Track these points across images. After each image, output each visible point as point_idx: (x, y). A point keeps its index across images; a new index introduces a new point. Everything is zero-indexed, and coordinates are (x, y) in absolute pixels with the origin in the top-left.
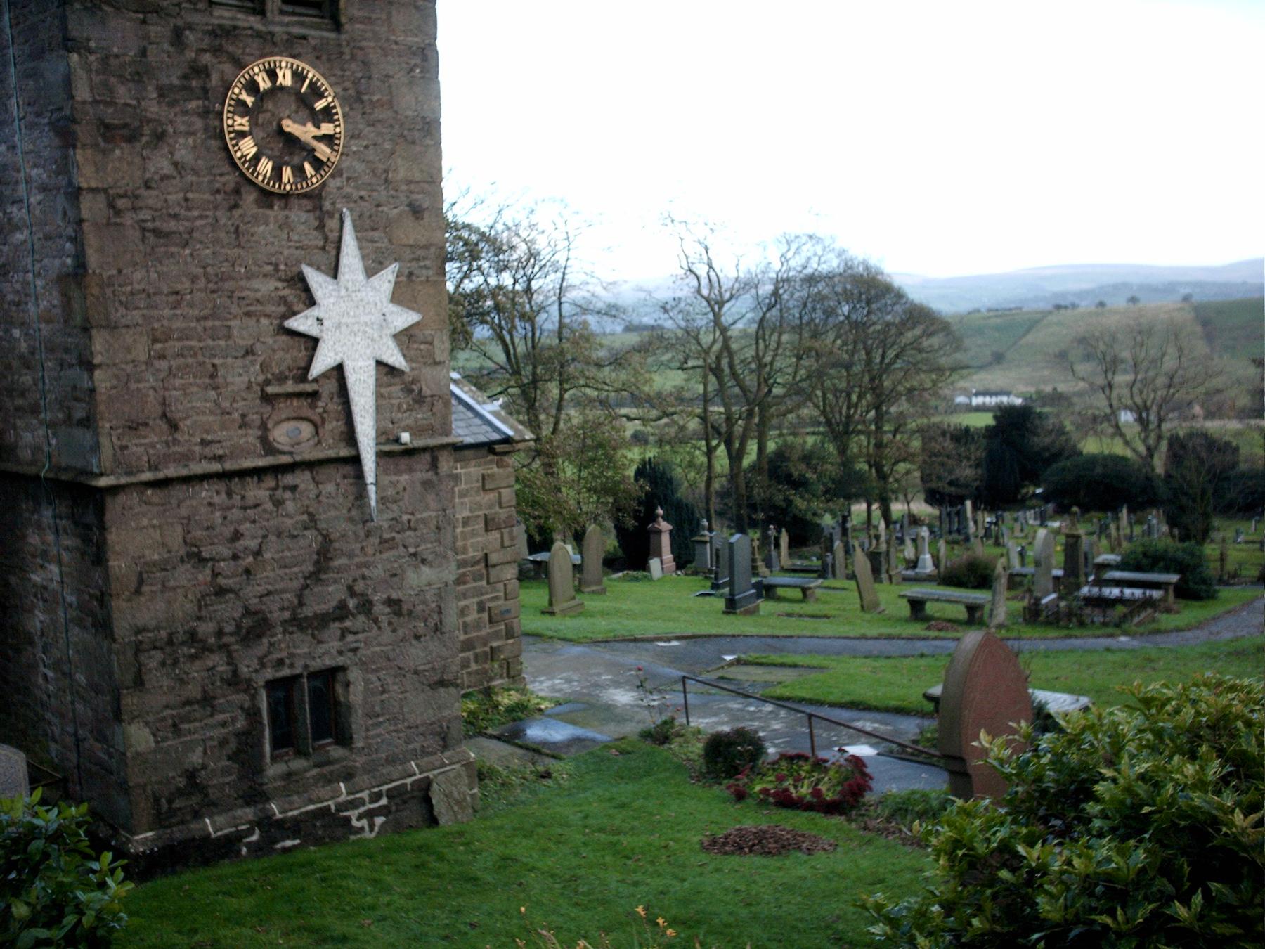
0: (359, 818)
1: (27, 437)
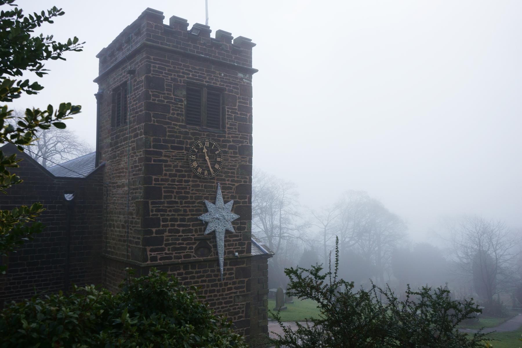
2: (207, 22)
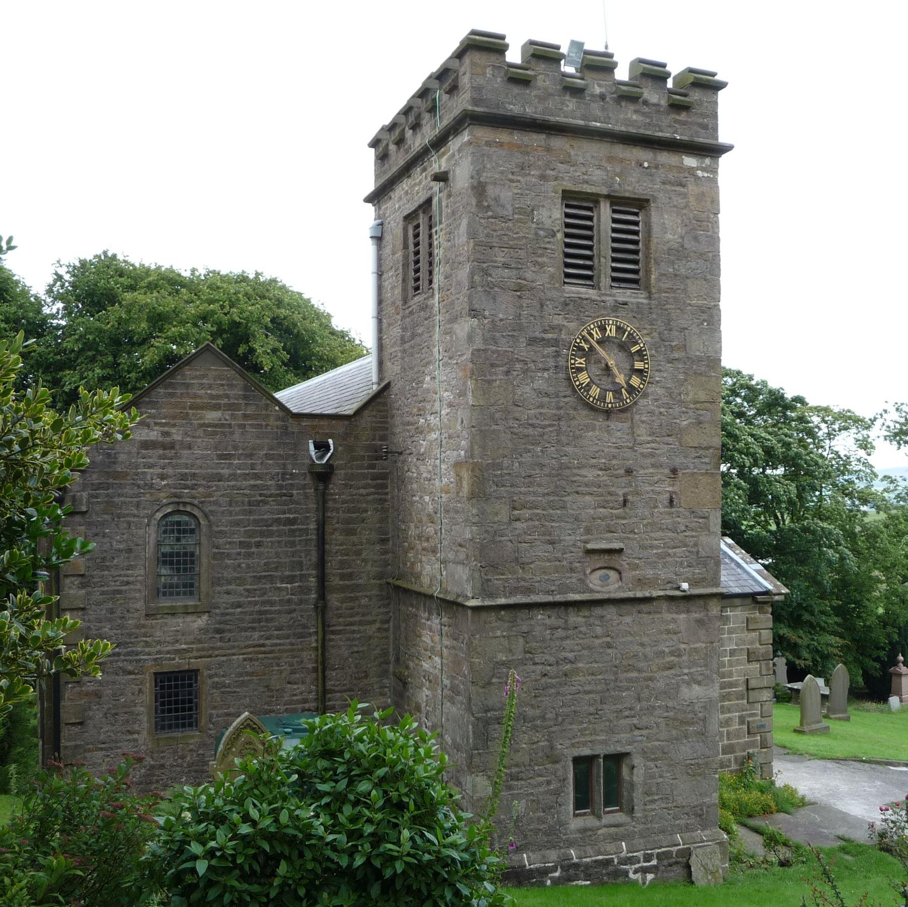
0: (636, 872)
1: (428, 568)
2: (606, 47)
